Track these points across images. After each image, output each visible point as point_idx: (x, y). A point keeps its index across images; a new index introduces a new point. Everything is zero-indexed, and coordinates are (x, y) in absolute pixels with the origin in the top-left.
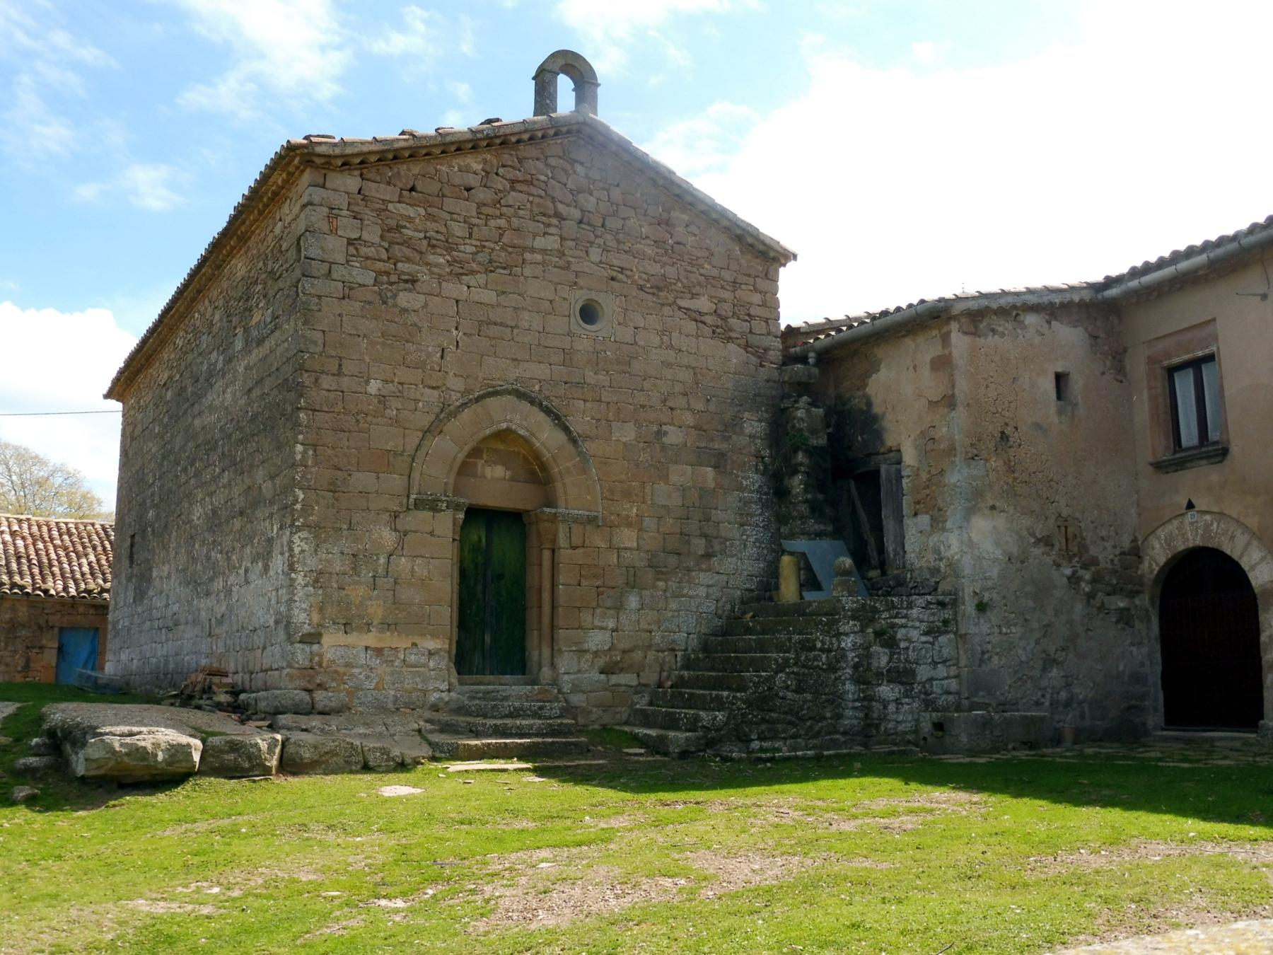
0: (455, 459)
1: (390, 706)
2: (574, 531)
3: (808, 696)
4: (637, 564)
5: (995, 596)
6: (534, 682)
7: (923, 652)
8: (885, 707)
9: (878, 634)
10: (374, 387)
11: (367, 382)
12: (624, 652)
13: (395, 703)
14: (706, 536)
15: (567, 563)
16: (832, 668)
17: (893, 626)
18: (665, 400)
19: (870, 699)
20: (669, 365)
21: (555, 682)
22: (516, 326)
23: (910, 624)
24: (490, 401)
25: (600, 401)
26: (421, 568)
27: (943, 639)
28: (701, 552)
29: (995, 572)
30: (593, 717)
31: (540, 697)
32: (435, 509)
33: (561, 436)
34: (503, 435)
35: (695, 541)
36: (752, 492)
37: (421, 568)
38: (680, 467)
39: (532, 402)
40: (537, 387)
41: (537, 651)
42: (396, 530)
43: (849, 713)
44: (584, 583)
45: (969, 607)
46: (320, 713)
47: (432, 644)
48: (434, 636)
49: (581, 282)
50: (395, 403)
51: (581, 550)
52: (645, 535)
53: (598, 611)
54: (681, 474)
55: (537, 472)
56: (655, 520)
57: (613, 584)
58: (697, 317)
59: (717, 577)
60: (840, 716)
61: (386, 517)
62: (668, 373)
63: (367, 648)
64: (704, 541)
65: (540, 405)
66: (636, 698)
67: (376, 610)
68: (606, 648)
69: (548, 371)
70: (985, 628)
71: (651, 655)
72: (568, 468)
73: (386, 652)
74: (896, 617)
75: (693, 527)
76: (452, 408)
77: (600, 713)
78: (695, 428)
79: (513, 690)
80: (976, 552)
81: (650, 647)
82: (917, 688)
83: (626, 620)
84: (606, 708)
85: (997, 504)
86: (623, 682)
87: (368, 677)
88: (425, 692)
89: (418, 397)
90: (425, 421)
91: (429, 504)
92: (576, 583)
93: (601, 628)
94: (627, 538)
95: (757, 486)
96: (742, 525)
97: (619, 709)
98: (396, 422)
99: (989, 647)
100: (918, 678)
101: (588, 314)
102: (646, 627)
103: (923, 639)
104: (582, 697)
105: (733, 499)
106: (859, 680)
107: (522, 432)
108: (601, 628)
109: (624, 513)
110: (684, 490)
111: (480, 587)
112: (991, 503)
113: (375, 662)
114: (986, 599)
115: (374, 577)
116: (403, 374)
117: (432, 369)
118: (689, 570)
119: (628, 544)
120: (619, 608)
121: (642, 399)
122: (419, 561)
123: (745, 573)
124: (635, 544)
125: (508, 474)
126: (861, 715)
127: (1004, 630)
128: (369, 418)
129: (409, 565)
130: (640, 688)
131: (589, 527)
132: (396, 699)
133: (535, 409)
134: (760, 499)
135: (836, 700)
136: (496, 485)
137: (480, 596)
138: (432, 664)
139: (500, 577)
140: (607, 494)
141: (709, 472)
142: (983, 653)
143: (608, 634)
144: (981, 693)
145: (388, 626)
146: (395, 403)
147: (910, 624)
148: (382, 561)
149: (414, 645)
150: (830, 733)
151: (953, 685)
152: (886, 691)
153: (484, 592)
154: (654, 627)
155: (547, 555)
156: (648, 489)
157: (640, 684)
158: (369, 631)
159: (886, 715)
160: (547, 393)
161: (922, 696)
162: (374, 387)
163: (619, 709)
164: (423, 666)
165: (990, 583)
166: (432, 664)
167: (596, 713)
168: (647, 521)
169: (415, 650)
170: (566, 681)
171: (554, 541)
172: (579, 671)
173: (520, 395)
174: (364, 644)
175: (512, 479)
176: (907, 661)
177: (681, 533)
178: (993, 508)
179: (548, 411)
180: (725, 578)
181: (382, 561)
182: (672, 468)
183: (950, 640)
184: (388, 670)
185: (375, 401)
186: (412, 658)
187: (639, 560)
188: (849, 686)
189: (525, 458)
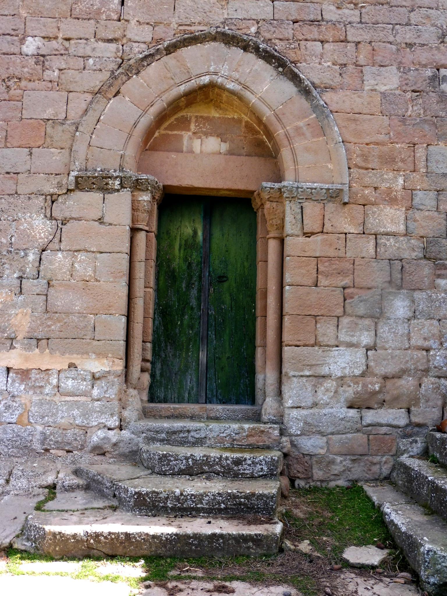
0: (135, 125)
1: (37, 446)
2: (307, 211)
4: (406, 255)
6: (257, 418)
10: (31, 46)
11: (22, 41)
12: (385, 378)
13: (43, 443)
15: (300, 253)
21: (279, 420)
25: (345, 41)
26: (83, 265)
30: (337, 469)
32: (105, 190)
33: (288, 88)
34: (206, 94)
37: (83, 265)
39: (245, 48)
40: (253, 29)
41: (266, 377)
42: (52, 218)
44: (323, 281)
47: (96, 366)
48: (100, 355)
50: (57, 63)
51: (319, 238)
52: (418, 215)
53: (345, 321)
55: (262, 144)
56: (433, 194)
57: (370, 284)
61: (40, 201)
63: (8, 370)
65: (257, 50)
66: (403, 443)
68: (357, 372)
69: (270, 9)
71: (428, 382)
72: (298, 129)
73: (33, 375)
76: (132, 62)
77: (348, 463)
79: (215, 429)
81: (426, 371)
83: (390, 334)
84: (357, 457)
86: (383, 420)
88: (85, 430)
89: (89, 53)
90: (96, 80)
92: (310, 282)
94: (390, 218)
97: (377, 459)
98: (56, 85)
102: (421, 343)
104: (321, 441)
107: (231, 86)
108: (350, 345)
109: (384, 186)
111: (194, 292)
113: (19, 388)
115: (21, 278)
116: (70, 28)
117: (109, 19)
119: (391, 228)
120: (377, 316)
121: (407, 35)
122: (81, 256)
125: (224, 147)
128: (23, 83)
129: (67, 262)
130: (411, 430)
131: (330, 207)
132: (44, 438)
133: (251, 57)
136: (203, 160)
137: (194, 302)
139: (222, 279)
140: (358, 161)
143: (360, 353)
145: (36, 341)
146: (57, 63)
148: (31, 257)
149: (72, 366)
153: (199, 299)
154: (433, 343)
155: (273, 245)
156: (420, 152)
157: (410, 424)
158: (12, 347)
160: (268, 36)
162: (31, 46)
163: (377, 459)
164: (85, 394)
166: (96, 392)
167: (340, 463)
168: (419, 196)
169: (73, 373)
170: (295, 421)
171: (281, 227)
172: (315, 405)
173: (229, 40)
175: (231, 153)
179: (268, 57)
181: (31, 257)
184: (35, 398)
185: (32, 61)
186: (69, 384)
187: (409, 250)
189: (248, 127)
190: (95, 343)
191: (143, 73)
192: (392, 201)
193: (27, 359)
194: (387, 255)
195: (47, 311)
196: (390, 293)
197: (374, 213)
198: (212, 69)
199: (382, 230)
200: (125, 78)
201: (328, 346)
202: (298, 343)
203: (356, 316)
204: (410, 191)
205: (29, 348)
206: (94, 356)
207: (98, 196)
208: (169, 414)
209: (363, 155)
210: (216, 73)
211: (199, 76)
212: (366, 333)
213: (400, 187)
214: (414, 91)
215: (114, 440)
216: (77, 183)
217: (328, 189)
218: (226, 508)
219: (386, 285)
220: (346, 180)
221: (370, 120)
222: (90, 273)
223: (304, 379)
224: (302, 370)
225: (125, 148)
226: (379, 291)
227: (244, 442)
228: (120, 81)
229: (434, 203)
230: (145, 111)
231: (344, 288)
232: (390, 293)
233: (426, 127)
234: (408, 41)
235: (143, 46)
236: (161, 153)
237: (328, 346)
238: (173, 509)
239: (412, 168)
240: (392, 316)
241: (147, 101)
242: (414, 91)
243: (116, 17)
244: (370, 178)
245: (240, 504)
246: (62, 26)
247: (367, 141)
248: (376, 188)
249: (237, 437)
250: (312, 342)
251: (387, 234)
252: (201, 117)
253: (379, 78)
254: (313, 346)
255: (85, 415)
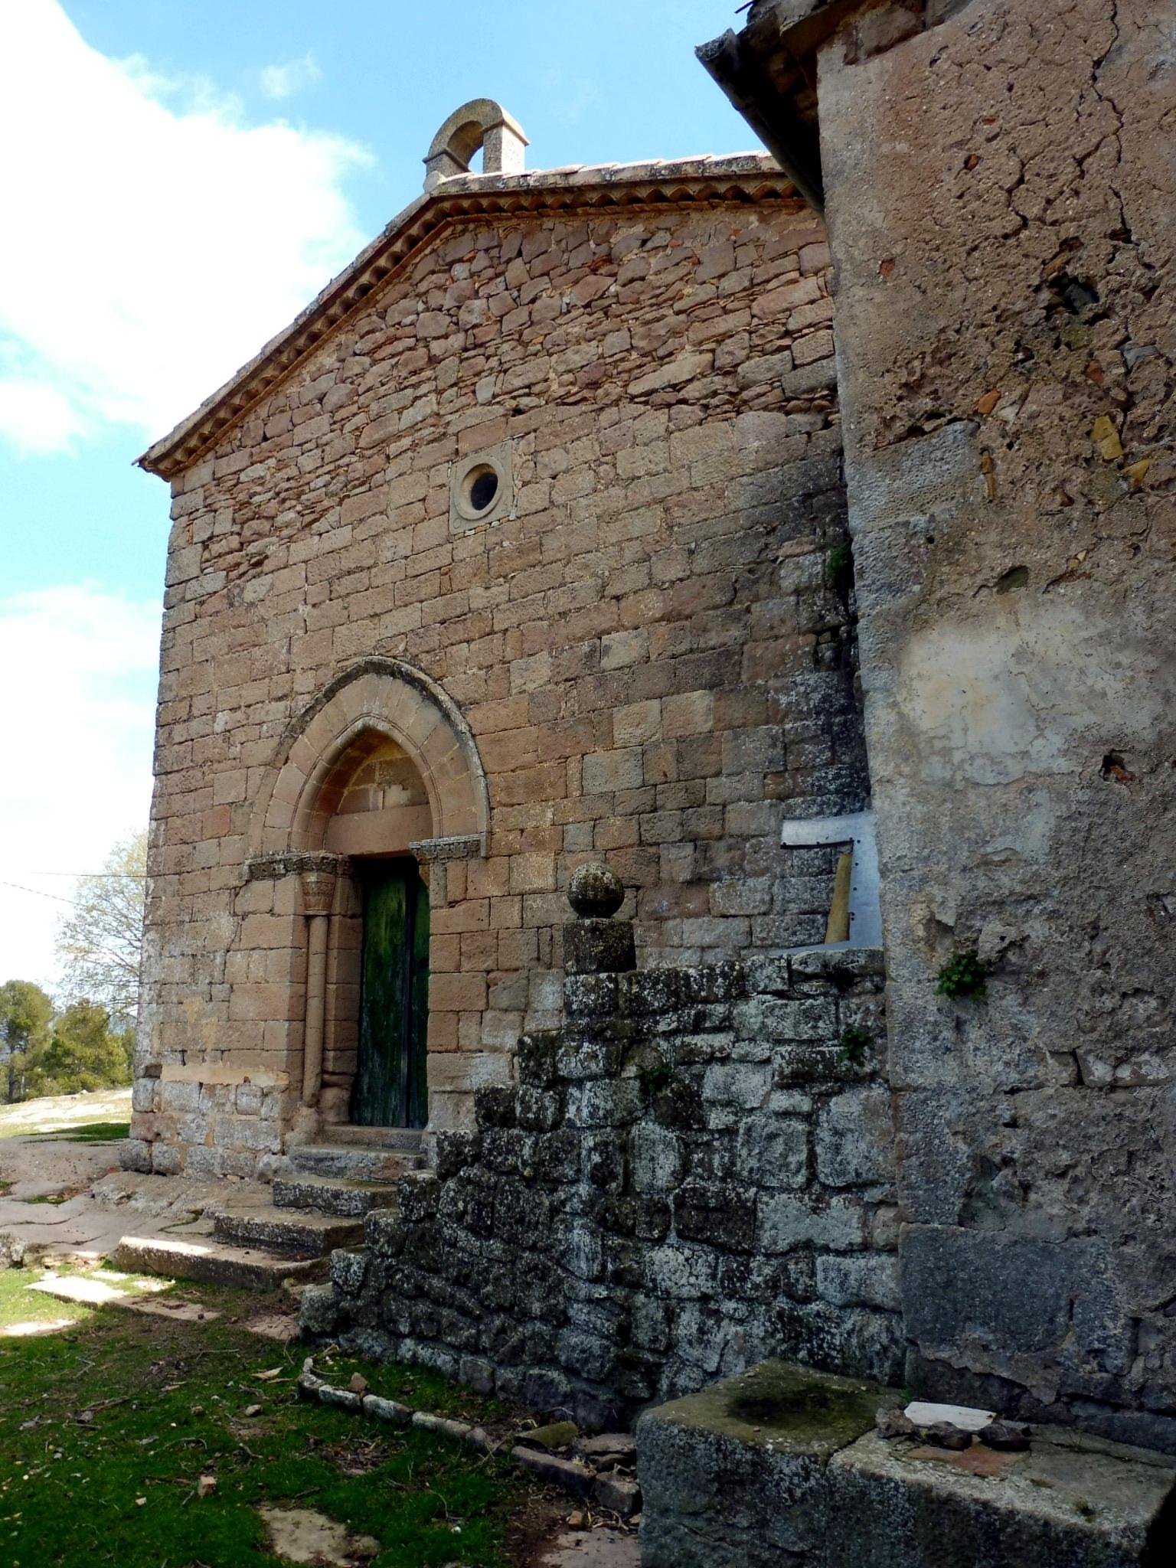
1: (217, 1170)
3: (496, 1246)
5: (1037, 930)
7: (779, 1146)
8: (671, 1318)
9: (652, 1082)
14: (694, 839)
16: (543, 1178)
17: (689, 1057)
18: (604, 587)
19: (631, 1281)
20: (613, 516)
22: (375, 565)
23: (742, 1048)
24: (346, 694)
25: (492, 633)
27: (846, 1106)
28: (685, 875)
29: (1036, 832)
31: (388, 1173)
32: (275, 876)
35: (670, 853)
36: (801, 716)
38: (635, 708)
42: (235, 915)
43: (579, 1313)
44: (466, 966)
45: (914, 990)
46: (158, 1173)
47: (265, 1080)
48: (269, 1067)
49: (464, 447)
50: (239, 736)
53: (488, 1016)
54: (637, 721)
57: (519, 964)
58: (673, 397)
59: (722, 926)
60: (563, 1320)
62: (612, 534)
63: (201, 1085)
64: (689, 849)
67: (210, 1032)
70: (988, 1063)
72: (442, 767)
74: (697, 1029)
75: (667, 824)
78: (667, 618)
80: (936, 769)
82: (761, 1271)
85: (1032, 557)
87: (199, 1127)
88: (255, 1153)
91: (262, 870)
92: (451, 966)
93: (495, 1050)
95: (816, 697)
96: (782, 798)
99: (1014, 1144)
100: (766, 1238)
101: (484, 488)
103: (781, 1101)
105: (756, 746)
106: (606, 1223)
108: (495, 1050)
110: (644, 753)
112: (1000, 562)
114: (988, 946)
115: (211, 983)
118: (662, 919)
119: (538, 883)
121: (561, 601)
122: (256, 955)
123: (793, 907)
124: (551, 880)
126: (609, 1327)
127: (1100, 1071)
131: (473, 864)
134: (827, 728)
135: (549, 1270)
138: (264, 1111)
140: (501, 797)
141: (699, 701)
142: (985, 1167)
144: (977, 1333)
147: (742, 1048)
148: (218, 960)
149: (246, 1080)
150: (539, 1361)
151: (883, 1278)
152: (672, 1264)
156: (573, 766)
158: (204, 1060)
159: (671, 1346)
161: (782, 1303)
165: (1008, 881)
174: (198, 1079)
176: (729, 1173)
177: (641, 843)
178: (1013, 577)
179: (411, 680)
180: (742, 925)
182: (620, 713)
183: (870, 1111)
186: (244, 1101)
188: (580, 1236)
190: (265, 1054)
191: (308, 730)
192: (539, 845)
193: (214, 1073)
194: (535, 922)
195: (229, 1020)
196: (537, 975)
197: (519, 865)
198: (365, 710)
199: (527, 887)
200: (291, 741)
201: (470, 1051)
202: (440, 1048)
203: (500, 1010)
204: (559, 825)
205: (215, 1061)
206: (263, 1069)
207: (268, 884)
208: (348, 1139)
209: (507, 788)
210: (368, 714)
211: (355, 721)
212: (510, 1032)
213: (548, 823)
214: (566, 680)
215: (274, 1167)
216: (251, 872)
217: (465, 843)
218: (282, 1243)
219: (534, 963)
220: (483, 826)
221: (515, 736)
222: (261, 974)
223: (446, 1096)
224: (443, 1084)
225: (291, 826)
226: (524, 973)
227: (380, 1175)
228: (286, 746)
229: (588, 839)
230: (309, 776)
231: (488, 972)
232: (537, 975)
233: (581, 729)
234: (561, 610)
235: (307, 697)
236: (356, 817)
237: (470, 1051)
238: (243, 1238)
239: (563, 794)
240: (540, 1007)
241: (310, 764)
242: (566, 680)
243: (284, 669)
244: (515, 817)
245: (294, 1239)
246: (244, 693)
247: (512, 767)
248: (522, 831)
249: (374, 1168)
250: (454, 1047)
251: (534, 893)
252: (385, 762)
253: (525, 674)
254: (455, 1052)
255: (255, 1136)
